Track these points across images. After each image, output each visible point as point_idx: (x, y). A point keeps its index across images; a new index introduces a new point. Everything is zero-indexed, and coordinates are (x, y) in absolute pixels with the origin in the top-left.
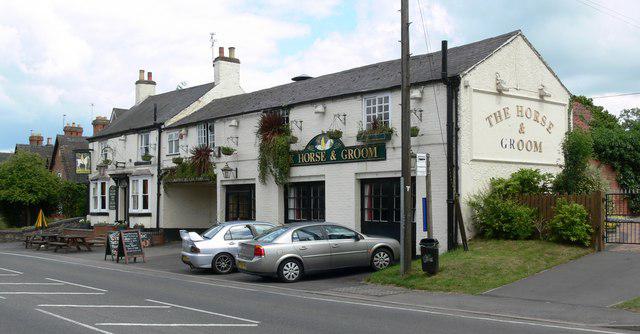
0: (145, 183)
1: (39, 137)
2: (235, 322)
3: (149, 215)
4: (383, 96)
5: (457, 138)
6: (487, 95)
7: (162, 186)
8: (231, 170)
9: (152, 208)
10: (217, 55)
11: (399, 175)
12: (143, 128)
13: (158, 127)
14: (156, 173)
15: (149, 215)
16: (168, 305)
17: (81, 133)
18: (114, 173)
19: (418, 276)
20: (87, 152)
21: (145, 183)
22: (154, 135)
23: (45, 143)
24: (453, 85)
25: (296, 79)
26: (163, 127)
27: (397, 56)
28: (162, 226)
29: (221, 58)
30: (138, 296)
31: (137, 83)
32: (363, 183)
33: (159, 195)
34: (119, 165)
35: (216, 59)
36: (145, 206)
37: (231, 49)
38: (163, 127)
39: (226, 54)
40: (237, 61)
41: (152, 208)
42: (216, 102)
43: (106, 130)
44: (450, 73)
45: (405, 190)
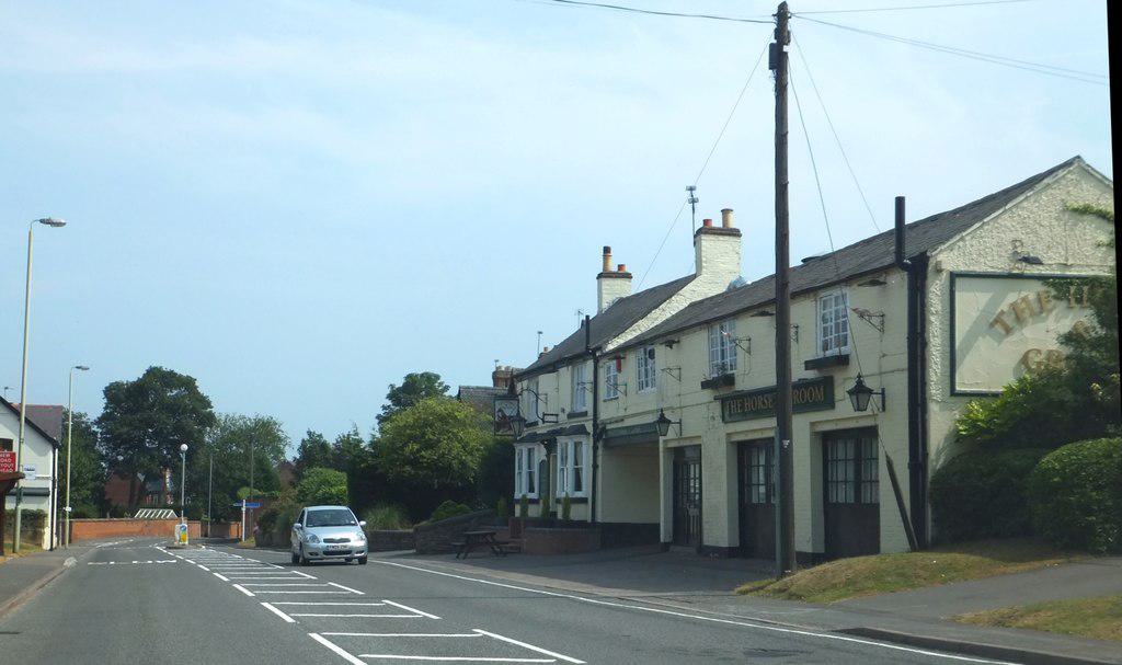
4: (836, 292)
6: (983, 280)
7: (600, 452)
8: (870, 392)
10: (700, 225)
11: (771, 434)
12: (716, 319)
15: (584, 501)
19: (182, 547)
22: (588, 367)
24: (918, 271)
25: (395, 395)
27: (891, 225)
28: (599, 519)
29: (706, 229)
31: (600, 276)
33: (595, 466)
34: (547, 418)
35: (699, 233)
36: (578, 487)
37: (725, 212)
39: (717, 223)
40: (735, 233)
41: (585, 492)
43: (550, 363)
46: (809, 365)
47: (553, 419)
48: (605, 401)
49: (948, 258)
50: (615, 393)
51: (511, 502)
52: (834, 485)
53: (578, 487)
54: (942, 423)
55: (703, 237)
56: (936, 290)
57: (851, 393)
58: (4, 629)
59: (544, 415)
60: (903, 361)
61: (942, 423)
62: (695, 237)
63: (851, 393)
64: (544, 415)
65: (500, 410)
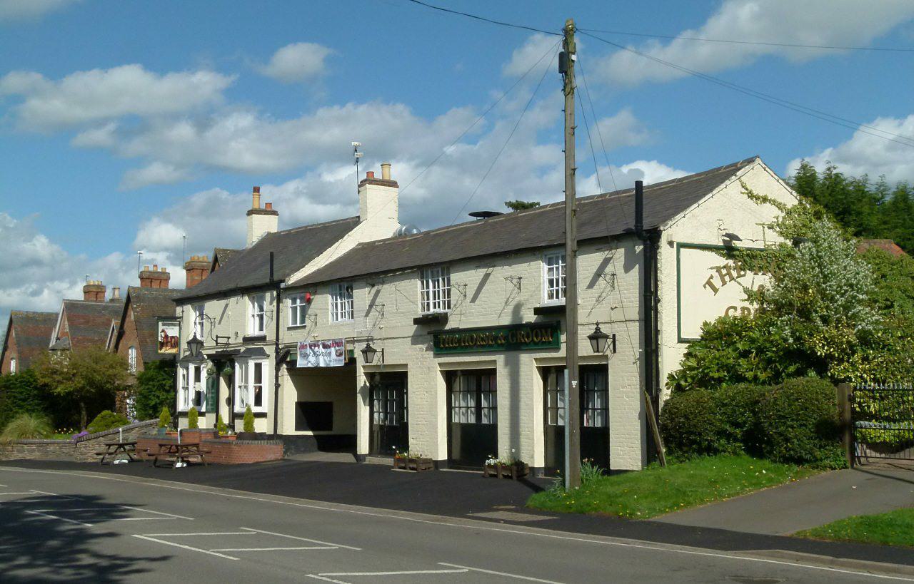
0: (258, 367)
1: (98, 286)
2: (321, 545)
3: (263, 415)
5: (656, 312)
9: (266, 406)
13: (274, 285)
14: (273, 355)
15: (263, 415)
16: (254, 532)
17: (168, 279)
18: (213, 352)
20: (172, 319)
21: (258, 367)
23: (108, 295)
26: (282, 285)
30: (235, 523)
32: (331, 430)
35: (362, 184)
36: (258, 401)
38: (282, 285)
41: (266, 406)
42: (366, 249)
44: (647, 224)
45: (570, 384)
46: (538, 311)
47: (224, 341)
48: (289, 329)
49: (678, 229)
50: (303, 321)
51: (176, 415)
52: (457, 409)
53: (258, 401)
54: (672, 359)
55: (368, 186)
56: (666, 255)
57: (591, 338)
58: (912, 485)
59: (217, 337)
60: (676, 325)
61: (672, 359)
62: (359, 186)
63: (591, 338)
64: (217, 337)
65: (163, 331)
